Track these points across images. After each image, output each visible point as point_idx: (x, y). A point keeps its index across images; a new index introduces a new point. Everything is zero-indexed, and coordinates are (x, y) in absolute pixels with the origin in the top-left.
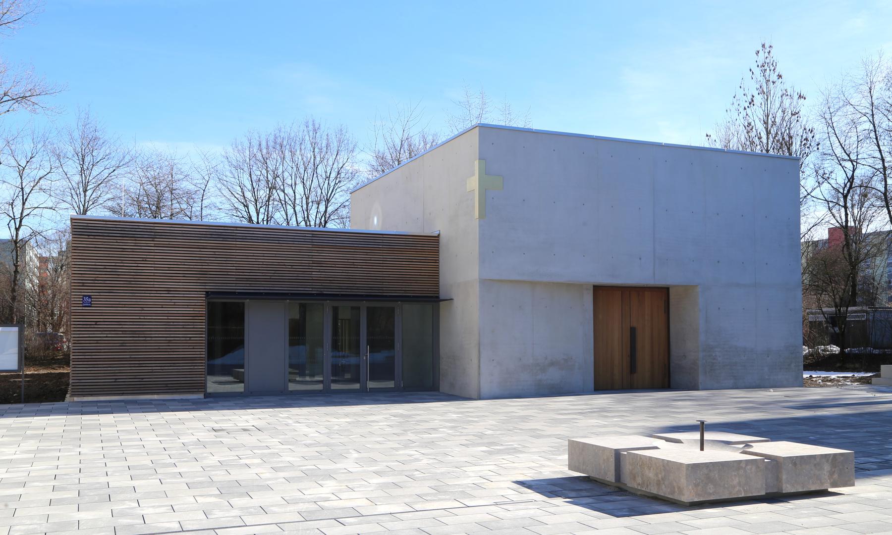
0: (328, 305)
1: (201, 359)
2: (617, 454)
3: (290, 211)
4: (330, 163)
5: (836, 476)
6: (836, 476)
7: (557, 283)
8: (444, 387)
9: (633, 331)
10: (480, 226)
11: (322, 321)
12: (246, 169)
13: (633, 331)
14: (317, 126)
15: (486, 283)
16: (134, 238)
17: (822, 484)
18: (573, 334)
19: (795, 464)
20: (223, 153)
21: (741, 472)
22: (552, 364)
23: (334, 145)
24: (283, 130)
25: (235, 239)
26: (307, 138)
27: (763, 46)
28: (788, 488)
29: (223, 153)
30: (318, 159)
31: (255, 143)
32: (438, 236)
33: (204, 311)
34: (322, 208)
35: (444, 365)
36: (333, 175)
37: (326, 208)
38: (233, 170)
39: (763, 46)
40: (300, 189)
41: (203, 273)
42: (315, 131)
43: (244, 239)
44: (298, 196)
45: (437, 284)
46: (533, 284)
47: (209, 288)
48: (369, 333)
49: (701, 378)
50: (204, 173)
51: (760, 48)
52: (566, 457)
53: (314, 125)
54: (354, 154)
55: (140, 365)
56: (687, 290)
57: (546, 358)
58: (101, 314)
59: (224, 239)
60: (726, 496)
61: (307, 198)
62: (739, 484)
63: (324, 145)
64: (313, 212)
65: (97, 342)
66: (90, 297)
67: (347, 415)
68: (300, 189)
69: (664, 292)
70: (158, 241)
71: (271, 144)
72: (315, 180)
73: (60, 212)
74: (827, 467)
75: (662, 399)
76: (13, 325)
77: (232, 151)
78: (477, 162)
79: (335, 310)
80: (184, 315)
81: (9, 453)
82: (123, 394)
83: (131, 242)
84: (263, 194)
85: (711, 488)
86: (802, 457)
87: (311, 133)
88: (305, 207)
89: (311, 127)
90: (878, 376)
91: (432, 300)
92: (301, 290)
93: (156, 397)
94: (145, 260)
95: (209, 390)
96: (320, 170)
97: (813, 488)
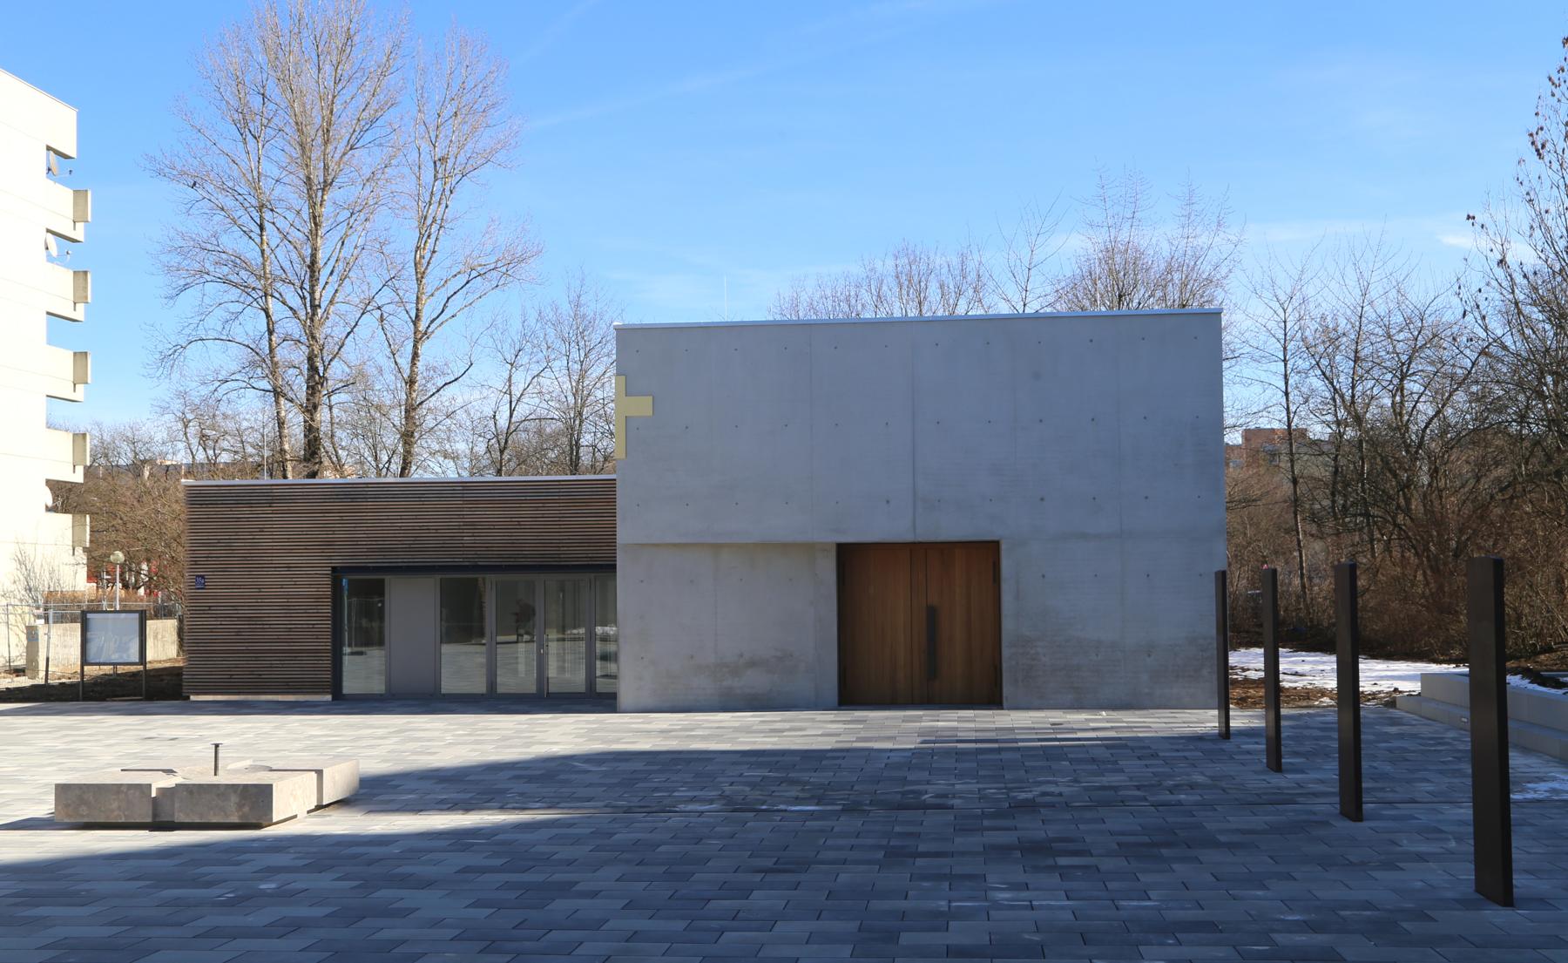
6: (246, 809)
7: (755, 545)
9: (932, 614)
13: (932, 614)
16: (250, 504)
17: (226, 815)
18: (807, 616)
19: (191, 793)
21: (122, 796)
22: (752, 664)
25: (365, 499)
28: (180, 817)
32: (65, 497)
41: (329, 543)
46: (716, 548)
47: (337, 562)
49: (1007, 690)
52: (1466, 812)
58: (214, 597)
59: (353, 500)
69: (988, 552)
70: (276, 507)
74: (234, 799)
75: (61, 728)
80: (309, 597)
83: (245, 512)
85: (84, 810)
86: (200, 786)
97: (214, 820)
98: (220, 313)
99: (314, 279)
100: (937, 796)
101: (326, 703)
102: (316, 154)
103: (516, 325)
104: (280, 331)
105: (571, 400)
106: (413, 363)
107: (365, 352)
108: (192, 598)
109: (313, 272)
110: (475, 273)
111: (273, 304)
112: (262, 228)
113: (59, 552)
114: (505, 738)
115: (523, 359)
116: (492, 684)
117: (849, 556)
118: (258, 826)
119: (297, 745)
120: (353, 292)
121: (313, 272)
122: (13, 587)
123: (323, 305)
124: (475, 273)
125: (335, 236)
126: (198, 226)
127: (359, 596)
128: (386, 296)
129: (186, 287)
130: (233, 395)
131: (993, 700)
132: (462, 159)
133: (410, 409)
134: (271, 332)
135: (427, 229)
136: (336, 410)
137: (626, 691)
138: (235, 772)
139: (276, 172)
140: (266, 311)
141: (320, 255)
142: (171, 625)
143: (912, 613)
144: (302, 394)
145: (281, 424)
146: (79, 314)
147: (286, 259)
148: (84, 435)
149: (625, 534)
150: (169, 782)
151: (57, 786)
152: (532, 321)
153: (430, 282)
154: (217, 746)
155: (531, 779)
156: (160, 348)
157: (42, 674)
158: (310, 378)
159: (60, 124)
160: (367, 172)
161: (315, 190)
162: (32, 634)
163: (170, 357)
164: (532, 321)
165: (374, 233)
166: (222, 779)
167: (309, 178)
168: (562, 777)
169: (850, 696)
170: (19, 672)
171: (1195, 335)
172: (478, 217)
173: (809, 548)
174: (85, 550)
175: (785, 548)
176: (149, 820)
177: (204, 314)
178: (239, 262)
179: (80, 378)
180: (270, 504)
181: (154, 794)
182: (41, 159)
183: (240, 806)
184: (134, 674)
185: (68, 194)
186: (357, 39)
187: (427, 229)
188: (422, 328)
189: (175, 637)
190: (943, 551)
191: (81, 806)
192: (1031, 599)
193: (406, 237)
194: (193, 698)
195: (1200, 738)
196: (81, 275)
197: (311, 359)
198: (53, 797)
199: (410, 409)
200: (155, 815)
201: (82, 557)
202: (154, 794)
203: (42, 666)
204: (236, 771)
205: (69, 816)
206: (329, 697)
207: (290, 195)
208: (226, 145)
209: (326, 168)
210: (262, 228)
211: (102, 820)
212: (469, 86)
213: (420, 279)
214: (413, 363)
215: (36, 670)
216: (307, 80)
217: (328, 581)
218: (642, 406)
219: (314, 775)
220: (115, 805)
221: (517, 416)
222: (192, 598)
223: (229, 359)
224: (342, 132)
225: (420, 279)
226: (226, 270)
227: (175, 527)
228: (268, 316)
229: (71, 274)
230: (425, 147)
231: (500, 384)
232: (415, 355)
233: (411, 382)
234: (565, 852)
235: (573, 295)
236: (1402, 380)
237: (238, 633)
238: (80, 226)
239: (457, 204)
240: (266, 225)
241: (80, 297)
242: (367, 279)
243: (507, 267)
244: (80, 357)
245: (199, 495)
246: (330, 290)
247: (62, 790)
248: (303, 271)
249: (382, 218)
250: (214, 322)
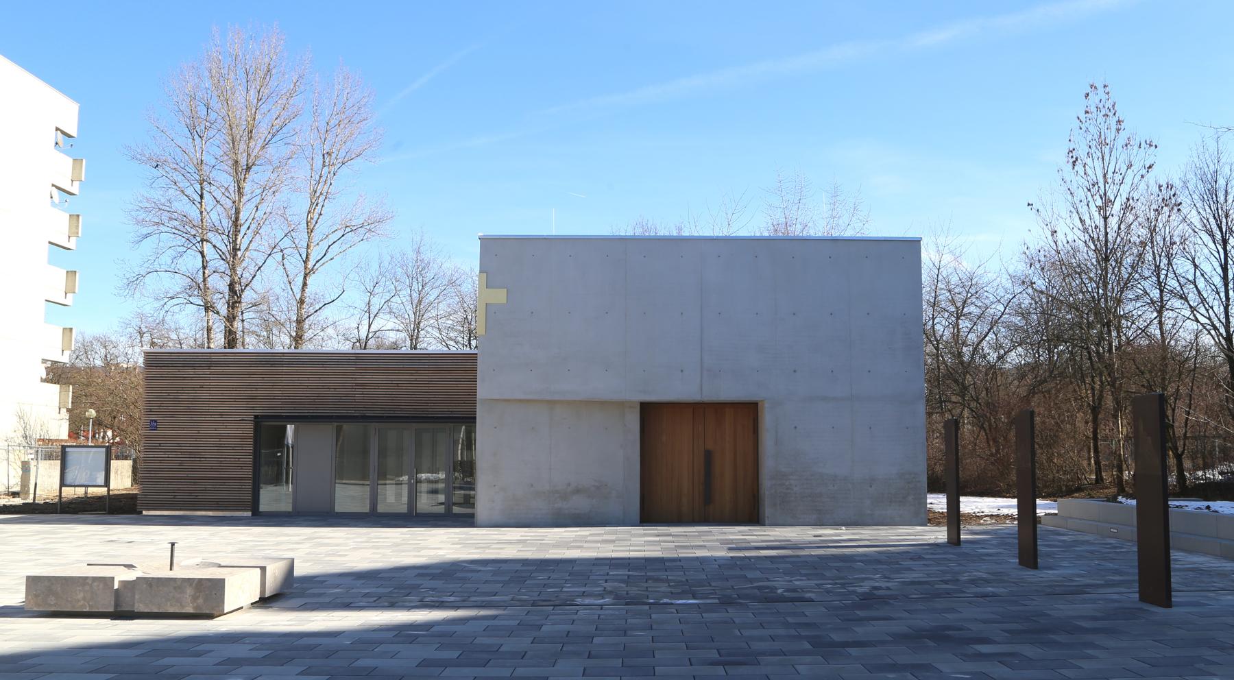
6: (200, 601)
13: (708, 456)
16: (193, 367)
17: (183, 607)
18: (616, 457)
19: (150, 585)
21: (87, 588)
22: (578, 491)
25: (281, 364)
32: (57, 374)
41: (253, 398)
46: (551, 403)
47: (258, 412)
49: (767, 511)
51: (1088, 90)
55: (195, 484)
62: (84, 599)
69: (749, 411)
74: (189, 591)
75: (39, 533)
81: (1229, 598)
85: (52, 600)
92: (343, 412)
93: (210, 513)
95: (262, 508)
97: (171, 610)
98: (171, 253)
99: (237, 232)
100: (787, 590)
101: (246, 518)
102: (242, 147)
103: (375, 266)
104: (212, 265)
105: (412, 316)
106: (303, 290)
107: (270, 282)
108: (147, 437)
109: (236, 226)
110: (349, 228)
111: (207, 248)
112: (202, 196)
113: (50, 414)
114: (397, 545)
115: (378, 290)
116: (374, 505)
117: (650, 412)
118: (210, 617)
119: (230, 548)
120: (262, 243)
121: (236, 226)
122: (13, 435)
123: (243, 248)
124: (349, 228)
125: (251, 205)
126: (157, 195)
128: (286, 243)
129: (147, 236)
130: (176, 309)
131: (753, 518)
132: (342, 153)
133: (300, 322)
134: (204, 268)
135: (316, 199)
136: (249, 318)
137: (483, 507)
138: (188, 567)
139: (213, 162)
140: (202, 253)
141: (241, 216)
142: (128, 464)
143: (695, 455)
144: (224, 310)
145: (209, 330)
146: (72, 244)
147: (218, 216)
148: (71, 329)
149: (484, 391)
150: (131, 576)
151: (28, 578)
152: (386, 264)
153: (316, 236)
154: (173, 544)
155: (434, 577)
156: (128, 275)
157: (32, 496)
158: (231, 297)
159: (67, 113)
160: (276, 163)
161: (241, 171)
162: (25, 467)
163: (134, 283)
164: (386, 264)
165: (277, 204)
166: (178, 573)
167: (236, 162)
168: (459, 575)
169: (649, 515)
170: (15, 494)
172: (350, 196)
173: (621, 405)
174: (68, 410)
175: (603, 404)
176: (111, 609)
177: (158, 254)
178: (185, 219)
179: (70, 290)
181: (116, 587)
182: (52, 135)
183: (195, 598)
184: (100, 498)
185: (69, 161)
186: (274, 71)
187: (316, 199)
188: (310, 266)
189: (130, 473)
190: (718, 409)
191: (51, 597)
192: (785, 443)
193: (301, 204)
194: (144, 513)
195: (937, 545)
196: (75, 217)
197: (231, 286)
198: (24, 588)
199: (300, 322)
200: (116, 605)
201: (65, 415)
202: (116, 587)
203: (32, 491)
204: (188, 567)
205: (39, 605)
206: (249, 514)
207: (224, 178)
208: (179, 141)
209: (249, 155)
210: (202, 196)
211: (68, 609)
212: (349, 105)
213: (310, 231)
214: (303, 290)
215: (27, 493)
216: (239, 97)
217: (251, 425)
218: (500, 296)
219: (258, 570)
220: (80, 596)
221: (374, 328)
222: (147, 437)
223: (176, 284)
224: (262, 131)
225: (310, 231)
226: (176, 223)
227: (131, 396)
228: (203, 256)
229: (71, 160)
230: (317, 144)
231: (363, 306)
232: (305, 284)
233: (302, 302)
234: (509, 645)
235: (416, 247)
236: (958, 318)
237: (181, 464)
238: (76, 184)
239: (338, 184)
240: (206, 195)
241: (73, 233)
242: (273, 232)
243: (369, 227)
244: (71, 274)
245: (155, 359)
246: (245, 242)
247: (33, 582)
248: (227, 223)
249: (284, 194)
250: (166, 259)
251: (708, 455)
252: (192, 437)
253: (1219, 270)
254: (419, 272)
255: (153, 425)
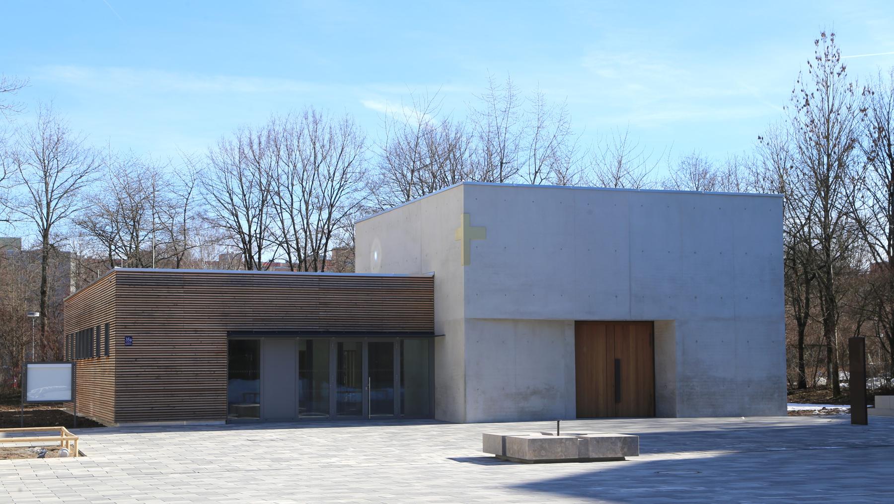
0: (334, 340)
1: (223, 389)
2: (504, 438)
3: (286, 216)
4: (334, 161)
5: (626, 450)
6: (626, 450)
8: (438, 415)
10: (465, 272)
11: (328, 358)
12: (235, 173)
14: (318, 117)
15: (471, 322)
16: (167, 286)
18: (556, 364)
20: (209, 155)
22: (535, 393)
23: (339, 139)
24: (277, 122)
26: (306, 132)
27: (823, 35)
28: (593, 455)
29: (209, 155)
30: (319, 158)
31: (245, 141)
33: (225, 348)
34: (325, 215)
35: (438, 395)
36: (338, 176)
37: (330, 214)
38: (221, 174)
39: (823, 35)
40: (298, 189)
41: (225, 315)
42: (316, 122)
43: (259, 284)
44: (295, 199)
45: (432, 321)
46: (515, 321)
47: (231, 328)
48: (370, 367)
49: (678, 407)
50: (188, 179)
51: (820, 37)
53: (314, 116)
54: (362, 150)
55: (173, 396)
56: (667, 323)
57: (528, 388)
59: (243, 285)
60: (553, 458)
61: (307, 203)
63: (327, 137)
64: (314, 219)
65: (137, 375)
66: (131, 337)
67: (349, 433)
68: (298, 189)
69: (647, 330)
71: (263, 139)
72: (316, 183)
73: (14, 223)
74: (619, 444)
76: (59, 360)
77: (218, 150)
78: (462, 216)
79: (340, 346)
82: (158, 420)
83: (164, 291)
84: (255, 197)
85: (543, 453)
87: (311, 126)
88: (304, 212)
89: (311, 119)
90: (874, 407)
91: (427, 334)
93: (185, 423)
94: (176, 305)
96: (323, 169)
97: (610, 456)
127: (243, 356)
169: (583, 413)
171: (18, 241)
180: (183, 286)
220: (559, 450)
245: (128, 278)
251: (617, 363)
252: (167, 352)
253: (617, 164)
254: (49, 155)
255: (128, 341)
